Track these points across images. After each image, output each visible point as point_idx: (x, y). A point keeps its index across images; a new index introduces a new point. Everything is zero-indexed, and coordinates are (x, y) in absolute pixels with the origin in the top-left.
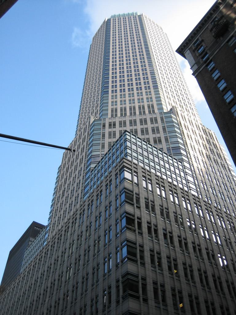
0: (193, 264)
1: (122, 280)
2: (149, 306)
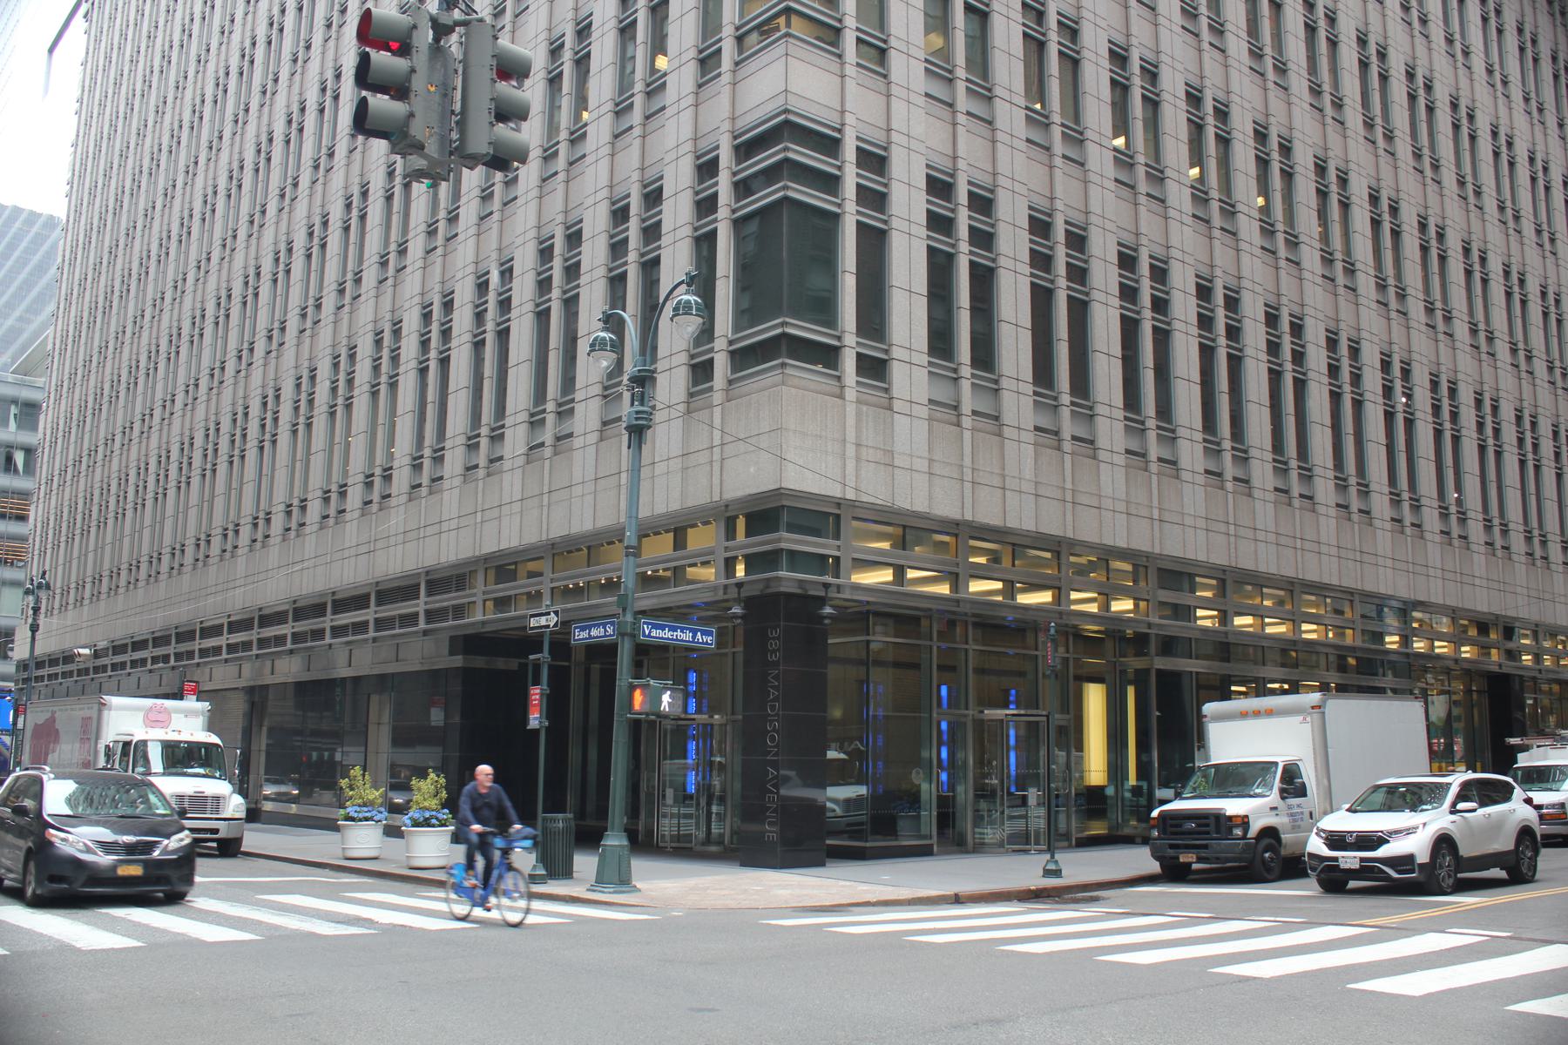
1: (735, 169)
2: (893, 86)
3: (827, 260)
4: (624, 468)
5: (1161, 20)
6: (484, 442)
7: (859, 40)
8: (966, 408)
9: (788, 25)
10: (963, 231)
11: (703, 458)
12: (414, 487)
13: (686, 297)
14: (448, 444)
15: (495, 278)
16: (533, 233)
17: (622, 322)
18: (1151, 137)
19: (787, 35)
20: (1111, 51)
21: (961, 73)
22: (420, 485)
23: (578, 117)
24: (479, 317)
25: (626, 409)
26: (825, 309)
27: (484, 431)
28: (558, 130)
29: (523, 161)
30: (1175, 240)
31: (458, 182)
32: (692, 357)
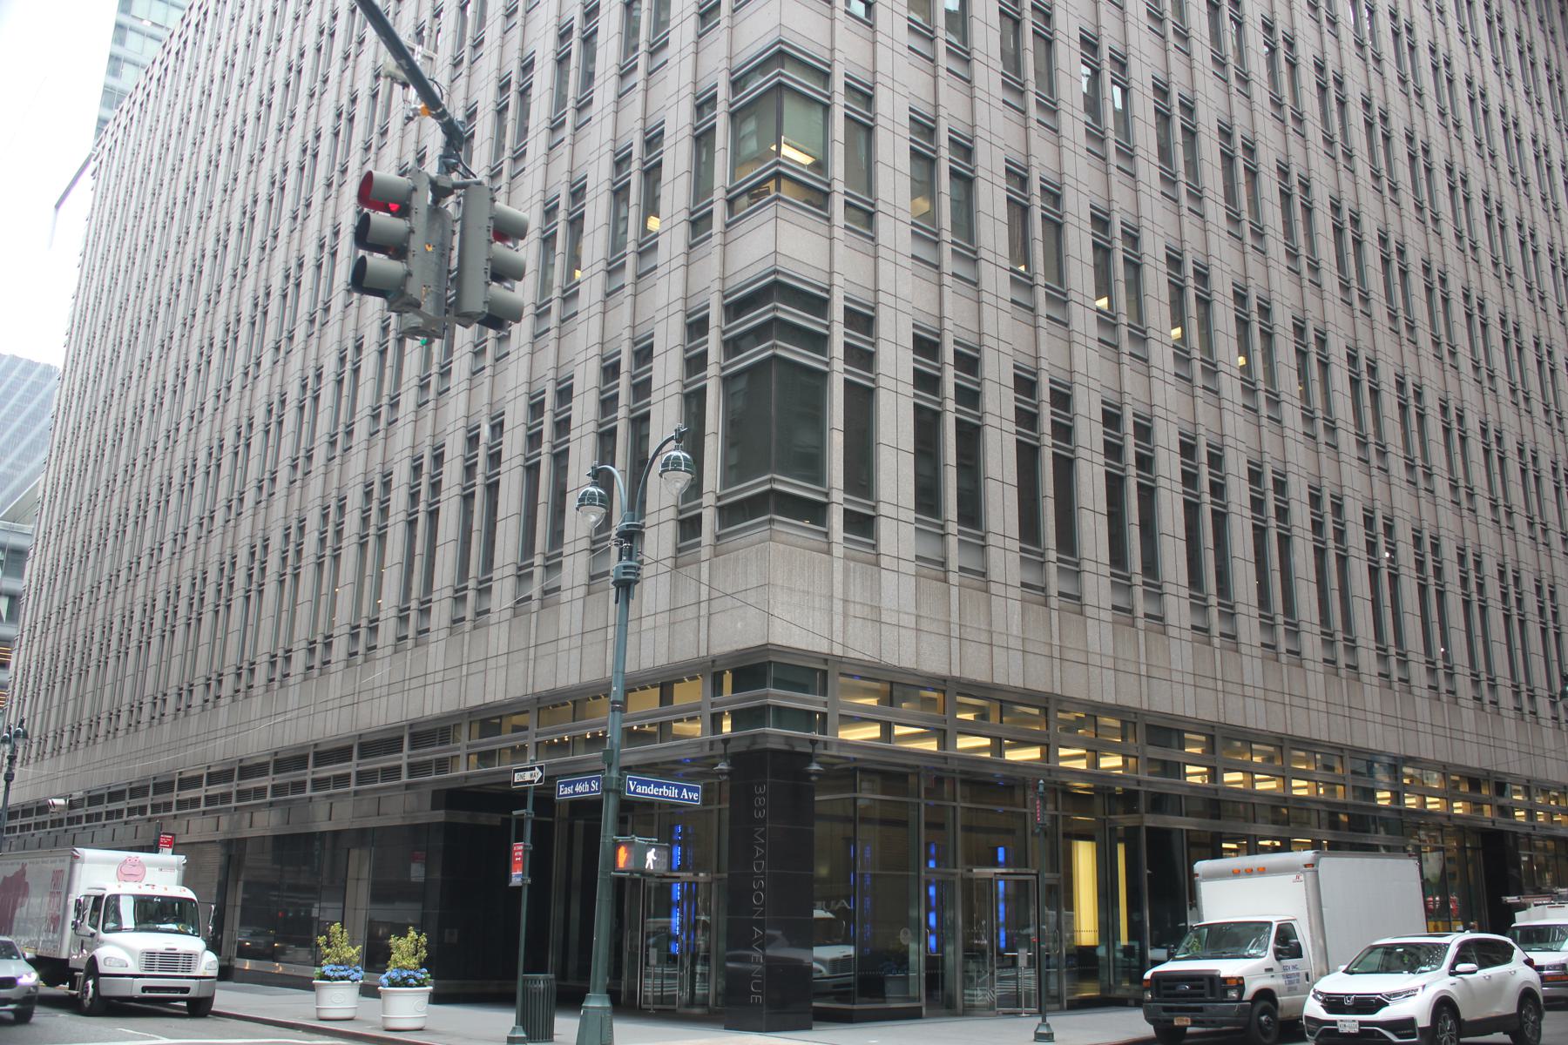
0: (1131, 50)
1: (725, 328)
9: (778, 188)
19: (777, 198)
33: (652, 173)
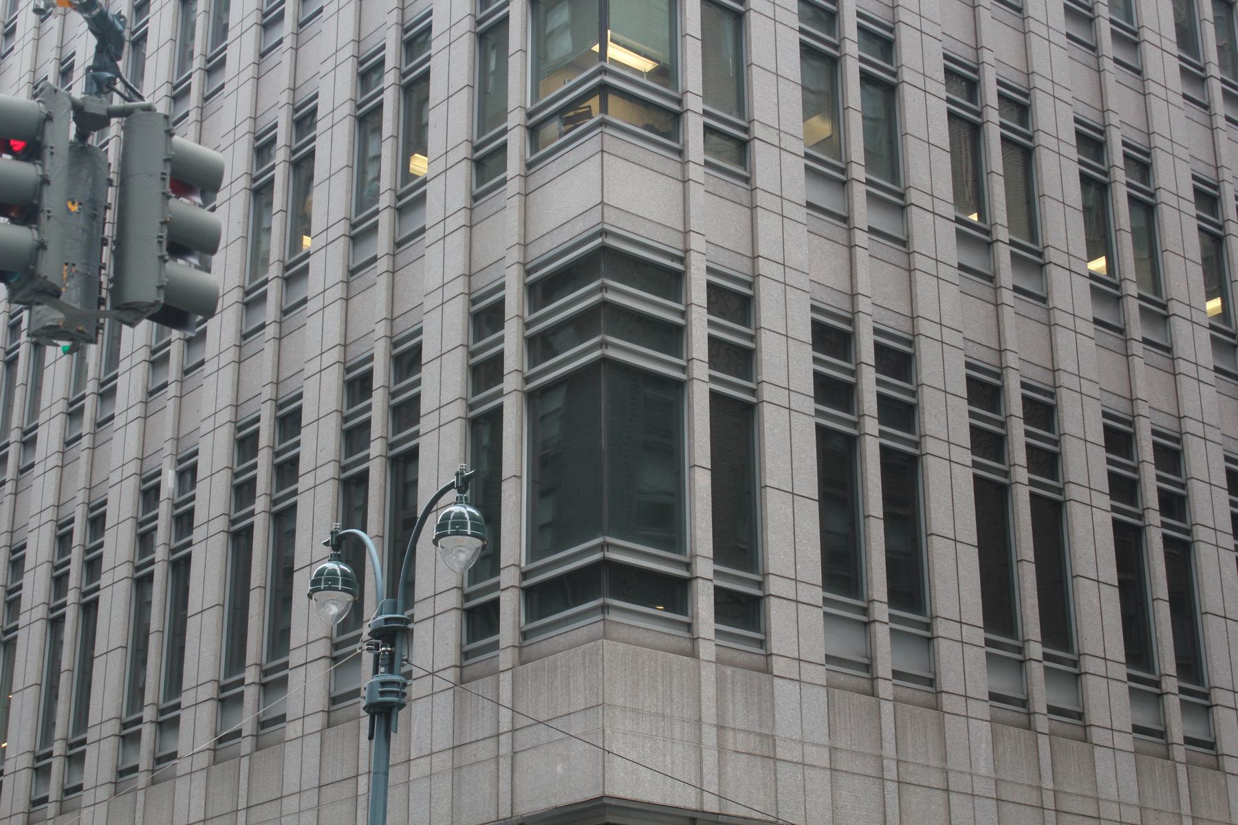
2: (760, 195)
3: (667, 445)
4: (364, 767)
5: (1152, 87)
6: (147, 731)
7: (708, 129)
8: (884, 667)
9: (604, 108)
10: (869, 403)
11: (484, 751)
12: (35, 803)
13: (456, 509)
14: (92, 735)
15: (169, 481)
16: (226, 415)
17: (360, 546)
18: (1145, 255)
19: (603, 123)
20: (1079, 134)
21: (858, 172)
22: (45, 800)
23: (295, 244)
24: (145, 540)
25: (366, 677)
26: (665, 522)
27: (148, 714)
28: (266, 263)
29: (209, 312)
30: (1189, 406)
31: (115, 340)
32: (467, 597)
33: (415, 90)
